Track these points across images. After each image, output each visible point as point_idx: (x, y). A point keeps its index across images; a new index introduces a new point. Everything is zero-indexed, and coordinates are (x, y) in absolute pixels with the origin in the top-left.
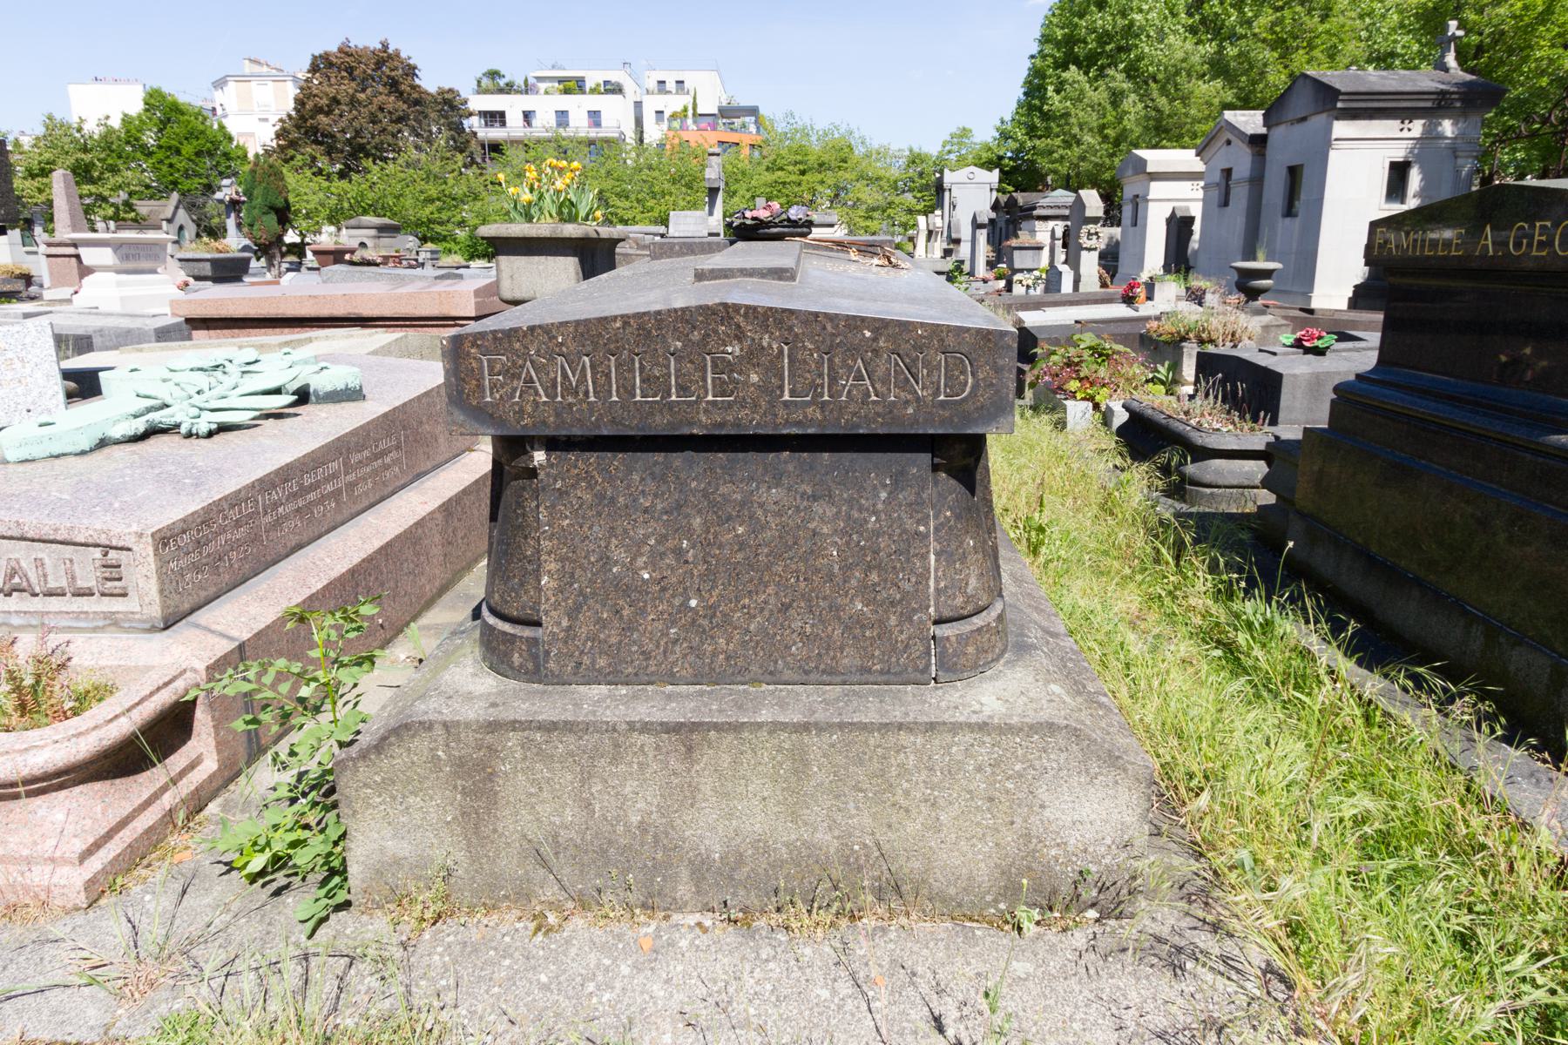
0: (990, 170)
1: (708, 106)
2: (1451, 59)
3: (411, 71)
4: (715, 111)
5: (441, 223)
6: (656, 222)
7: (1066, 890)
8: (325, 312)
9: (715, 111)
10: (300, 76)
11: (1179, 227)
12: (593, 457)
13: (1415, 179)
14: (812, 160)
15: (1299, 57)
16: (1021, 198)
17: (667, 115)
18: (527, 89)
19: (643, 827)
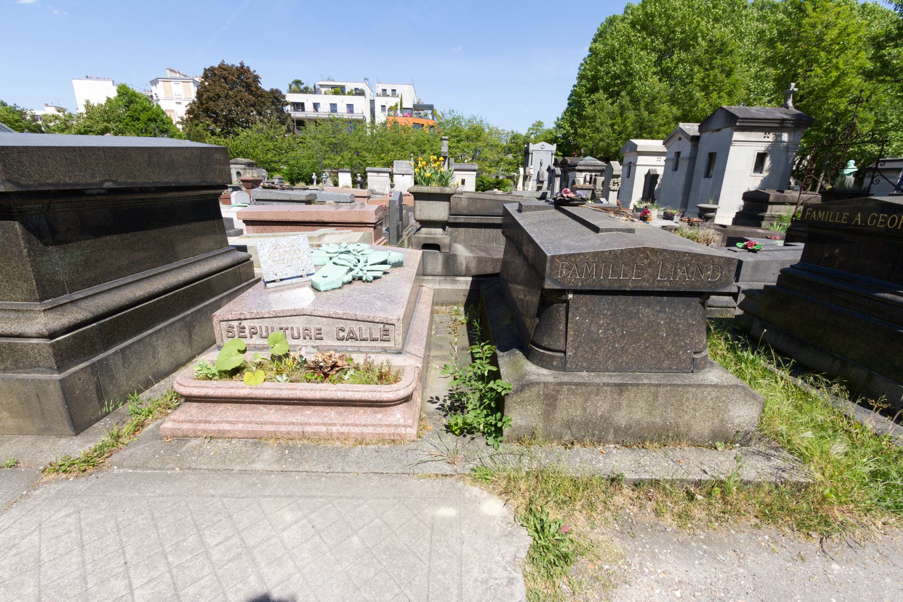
0: (551, 143)
1: (408, 104)
2: (790, 103)
3: (256, 79)
4: (411, 107)
5: (275, 162)
6: (385, 165)
7: (731, 438)
8: (308, 219)
9: (411, 107)
10: (197, 79)
11: (651, 179)
12: (588, 296)
13: (768, 163)
14: (463, 136)
15: (715, 95)
16: (569, 160)
17: (387, 108)
18: (315, 91)
19: (601, 417)
